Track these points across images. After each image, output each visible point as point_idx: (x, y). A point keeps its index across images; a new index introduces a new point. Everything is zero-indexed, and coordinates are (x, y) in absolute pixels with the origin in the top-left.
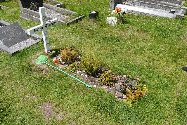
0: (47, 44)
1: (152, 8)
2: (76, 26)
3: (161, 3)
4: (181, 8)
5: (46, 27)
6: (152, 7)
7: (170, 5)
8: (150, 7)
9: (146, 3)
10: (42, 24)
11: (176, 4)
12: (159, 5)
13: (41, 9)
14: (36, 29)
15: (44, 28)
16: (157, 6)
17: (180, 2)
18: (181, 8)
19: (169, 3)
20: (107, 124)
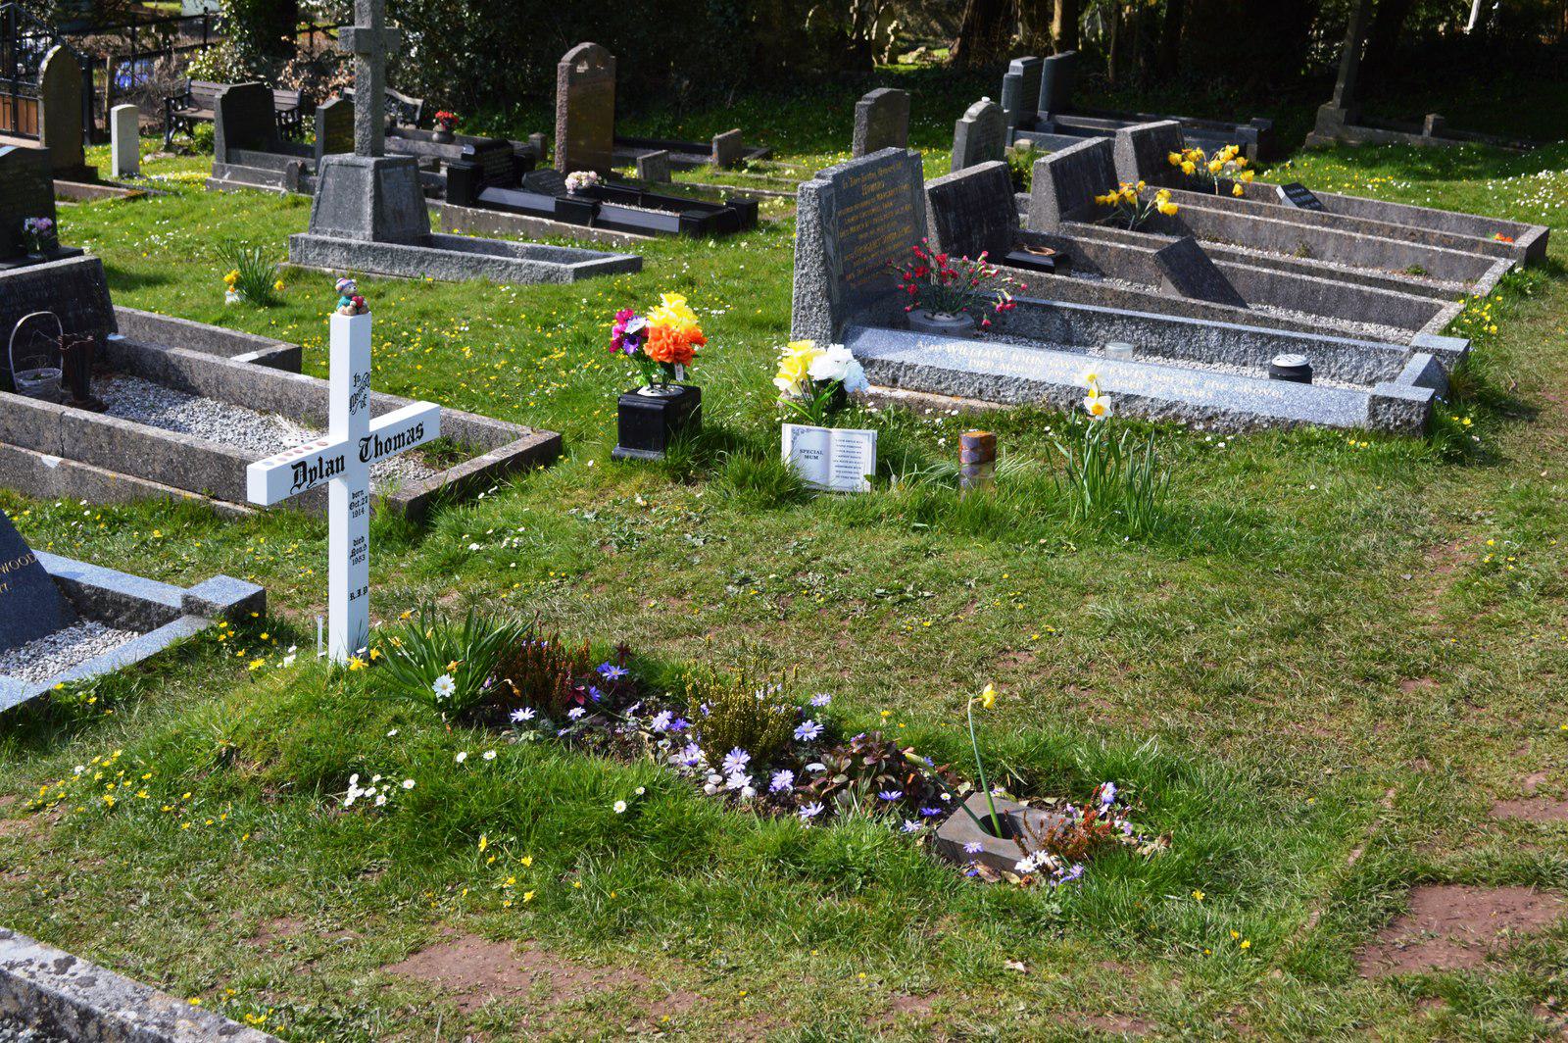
0: (352, 597)
1: (1173, 356)
2: (1441, 960)
3: (1252, 320)
4: (1415, 350)
5: (362, 459)
6: (1169, 353)
7: (1331, 332)
8: (1153, 352)
9: (1110, 319)
10: (339, 433)
11: (1392, 324)
12: (1224, 332)
13: (1139, 139)
14: (303, 464)
15: (352, 460)
16: (1214, 336)
17: (1421, 305)
18: (1415, 350)
19: (1326, 322)
20: (735, 1033)
